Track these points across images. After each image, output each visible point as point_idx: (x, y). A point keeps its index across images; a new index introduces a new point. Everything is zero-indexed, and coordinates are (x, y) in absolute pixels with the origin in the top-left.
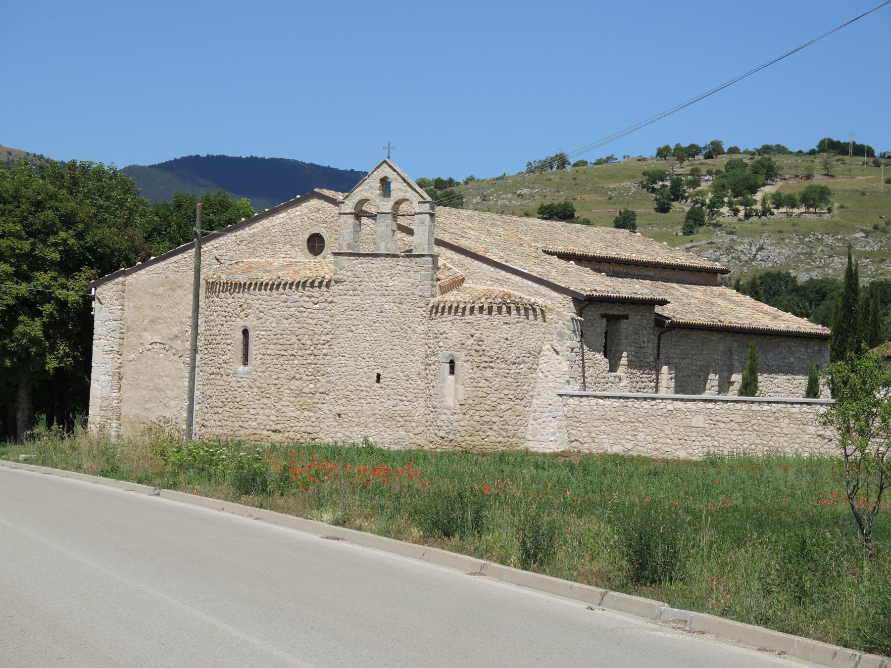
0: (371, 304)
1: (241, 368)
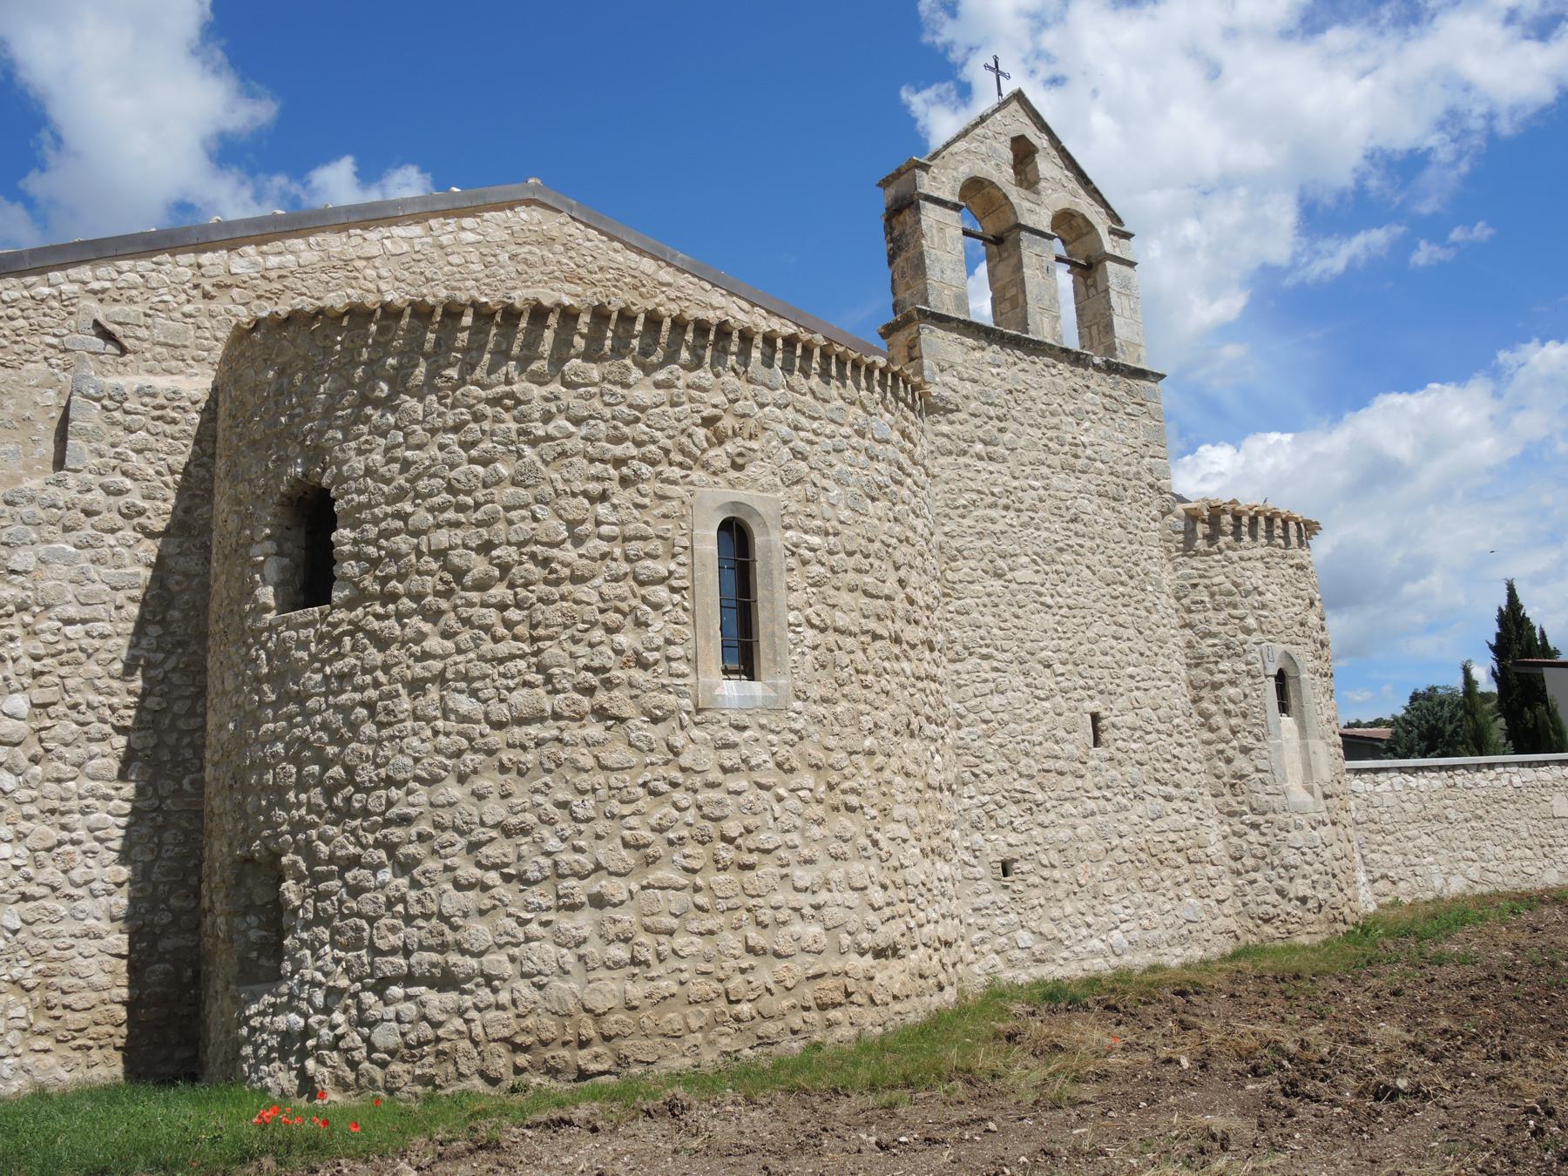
0: (1042, 492)
1: (732, 690)
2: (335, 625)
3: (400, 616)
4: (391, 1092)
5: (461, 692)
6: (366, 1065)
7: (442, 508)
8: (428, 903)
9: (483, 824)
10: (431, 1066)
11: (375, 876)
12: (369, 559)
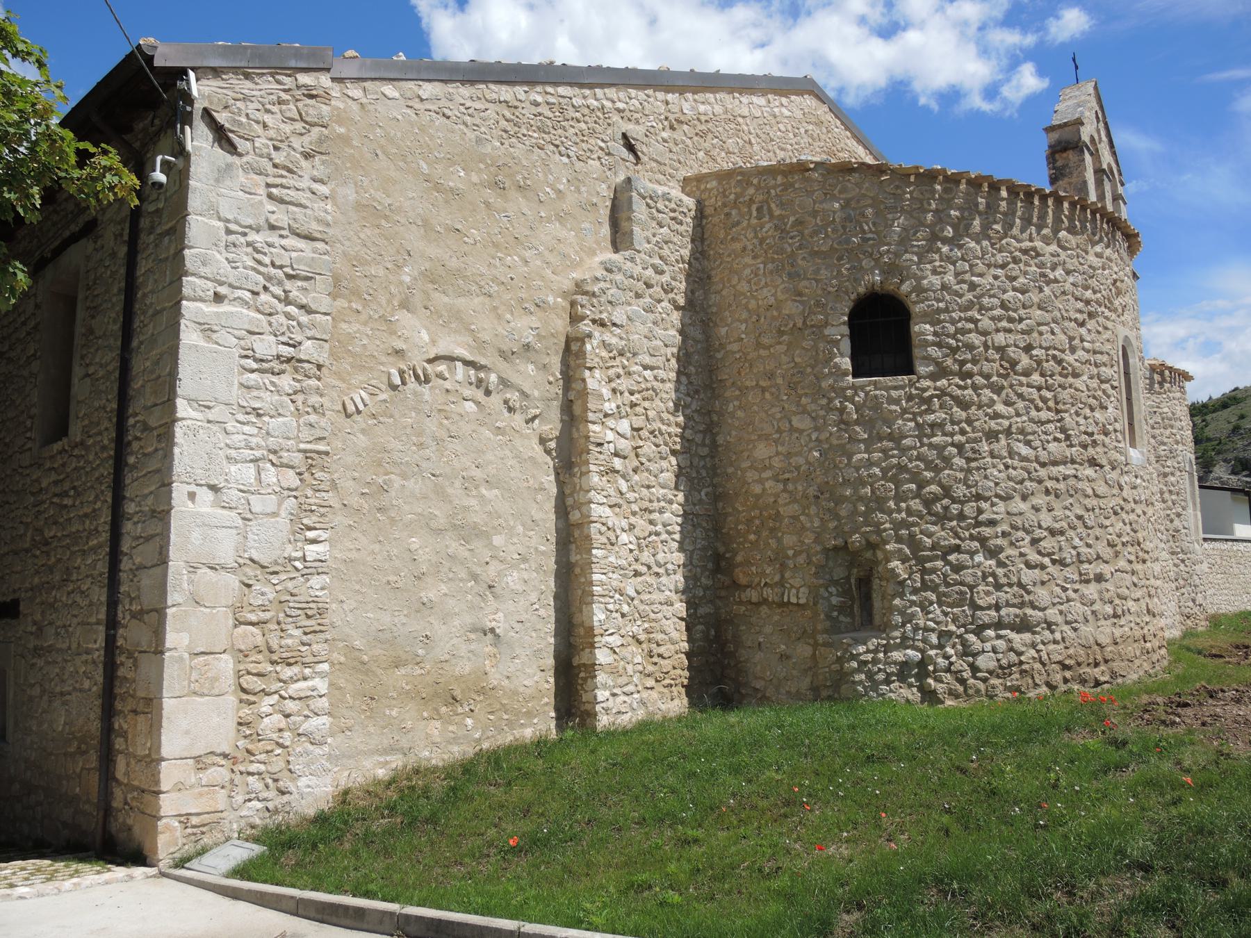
2: (924, 390)
3: (975, 387)
4: (991, 697)
5: (1020, 441)
6: (971, 681)
7: (1000, 319)
8: (1011, 576)
9: (1040, 527)
10: (1017, 680)
11: (972, 558)
12: (949, 347)
